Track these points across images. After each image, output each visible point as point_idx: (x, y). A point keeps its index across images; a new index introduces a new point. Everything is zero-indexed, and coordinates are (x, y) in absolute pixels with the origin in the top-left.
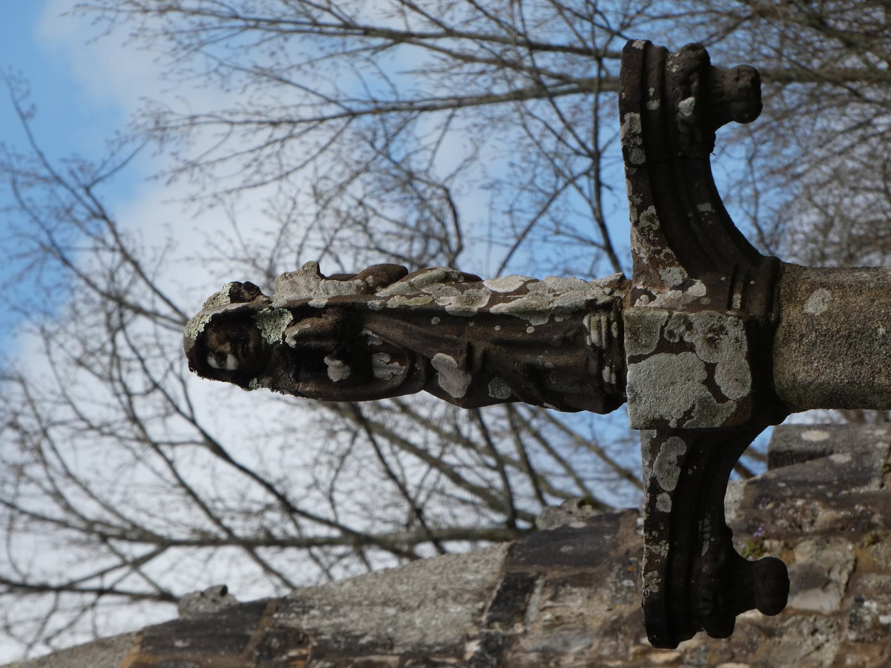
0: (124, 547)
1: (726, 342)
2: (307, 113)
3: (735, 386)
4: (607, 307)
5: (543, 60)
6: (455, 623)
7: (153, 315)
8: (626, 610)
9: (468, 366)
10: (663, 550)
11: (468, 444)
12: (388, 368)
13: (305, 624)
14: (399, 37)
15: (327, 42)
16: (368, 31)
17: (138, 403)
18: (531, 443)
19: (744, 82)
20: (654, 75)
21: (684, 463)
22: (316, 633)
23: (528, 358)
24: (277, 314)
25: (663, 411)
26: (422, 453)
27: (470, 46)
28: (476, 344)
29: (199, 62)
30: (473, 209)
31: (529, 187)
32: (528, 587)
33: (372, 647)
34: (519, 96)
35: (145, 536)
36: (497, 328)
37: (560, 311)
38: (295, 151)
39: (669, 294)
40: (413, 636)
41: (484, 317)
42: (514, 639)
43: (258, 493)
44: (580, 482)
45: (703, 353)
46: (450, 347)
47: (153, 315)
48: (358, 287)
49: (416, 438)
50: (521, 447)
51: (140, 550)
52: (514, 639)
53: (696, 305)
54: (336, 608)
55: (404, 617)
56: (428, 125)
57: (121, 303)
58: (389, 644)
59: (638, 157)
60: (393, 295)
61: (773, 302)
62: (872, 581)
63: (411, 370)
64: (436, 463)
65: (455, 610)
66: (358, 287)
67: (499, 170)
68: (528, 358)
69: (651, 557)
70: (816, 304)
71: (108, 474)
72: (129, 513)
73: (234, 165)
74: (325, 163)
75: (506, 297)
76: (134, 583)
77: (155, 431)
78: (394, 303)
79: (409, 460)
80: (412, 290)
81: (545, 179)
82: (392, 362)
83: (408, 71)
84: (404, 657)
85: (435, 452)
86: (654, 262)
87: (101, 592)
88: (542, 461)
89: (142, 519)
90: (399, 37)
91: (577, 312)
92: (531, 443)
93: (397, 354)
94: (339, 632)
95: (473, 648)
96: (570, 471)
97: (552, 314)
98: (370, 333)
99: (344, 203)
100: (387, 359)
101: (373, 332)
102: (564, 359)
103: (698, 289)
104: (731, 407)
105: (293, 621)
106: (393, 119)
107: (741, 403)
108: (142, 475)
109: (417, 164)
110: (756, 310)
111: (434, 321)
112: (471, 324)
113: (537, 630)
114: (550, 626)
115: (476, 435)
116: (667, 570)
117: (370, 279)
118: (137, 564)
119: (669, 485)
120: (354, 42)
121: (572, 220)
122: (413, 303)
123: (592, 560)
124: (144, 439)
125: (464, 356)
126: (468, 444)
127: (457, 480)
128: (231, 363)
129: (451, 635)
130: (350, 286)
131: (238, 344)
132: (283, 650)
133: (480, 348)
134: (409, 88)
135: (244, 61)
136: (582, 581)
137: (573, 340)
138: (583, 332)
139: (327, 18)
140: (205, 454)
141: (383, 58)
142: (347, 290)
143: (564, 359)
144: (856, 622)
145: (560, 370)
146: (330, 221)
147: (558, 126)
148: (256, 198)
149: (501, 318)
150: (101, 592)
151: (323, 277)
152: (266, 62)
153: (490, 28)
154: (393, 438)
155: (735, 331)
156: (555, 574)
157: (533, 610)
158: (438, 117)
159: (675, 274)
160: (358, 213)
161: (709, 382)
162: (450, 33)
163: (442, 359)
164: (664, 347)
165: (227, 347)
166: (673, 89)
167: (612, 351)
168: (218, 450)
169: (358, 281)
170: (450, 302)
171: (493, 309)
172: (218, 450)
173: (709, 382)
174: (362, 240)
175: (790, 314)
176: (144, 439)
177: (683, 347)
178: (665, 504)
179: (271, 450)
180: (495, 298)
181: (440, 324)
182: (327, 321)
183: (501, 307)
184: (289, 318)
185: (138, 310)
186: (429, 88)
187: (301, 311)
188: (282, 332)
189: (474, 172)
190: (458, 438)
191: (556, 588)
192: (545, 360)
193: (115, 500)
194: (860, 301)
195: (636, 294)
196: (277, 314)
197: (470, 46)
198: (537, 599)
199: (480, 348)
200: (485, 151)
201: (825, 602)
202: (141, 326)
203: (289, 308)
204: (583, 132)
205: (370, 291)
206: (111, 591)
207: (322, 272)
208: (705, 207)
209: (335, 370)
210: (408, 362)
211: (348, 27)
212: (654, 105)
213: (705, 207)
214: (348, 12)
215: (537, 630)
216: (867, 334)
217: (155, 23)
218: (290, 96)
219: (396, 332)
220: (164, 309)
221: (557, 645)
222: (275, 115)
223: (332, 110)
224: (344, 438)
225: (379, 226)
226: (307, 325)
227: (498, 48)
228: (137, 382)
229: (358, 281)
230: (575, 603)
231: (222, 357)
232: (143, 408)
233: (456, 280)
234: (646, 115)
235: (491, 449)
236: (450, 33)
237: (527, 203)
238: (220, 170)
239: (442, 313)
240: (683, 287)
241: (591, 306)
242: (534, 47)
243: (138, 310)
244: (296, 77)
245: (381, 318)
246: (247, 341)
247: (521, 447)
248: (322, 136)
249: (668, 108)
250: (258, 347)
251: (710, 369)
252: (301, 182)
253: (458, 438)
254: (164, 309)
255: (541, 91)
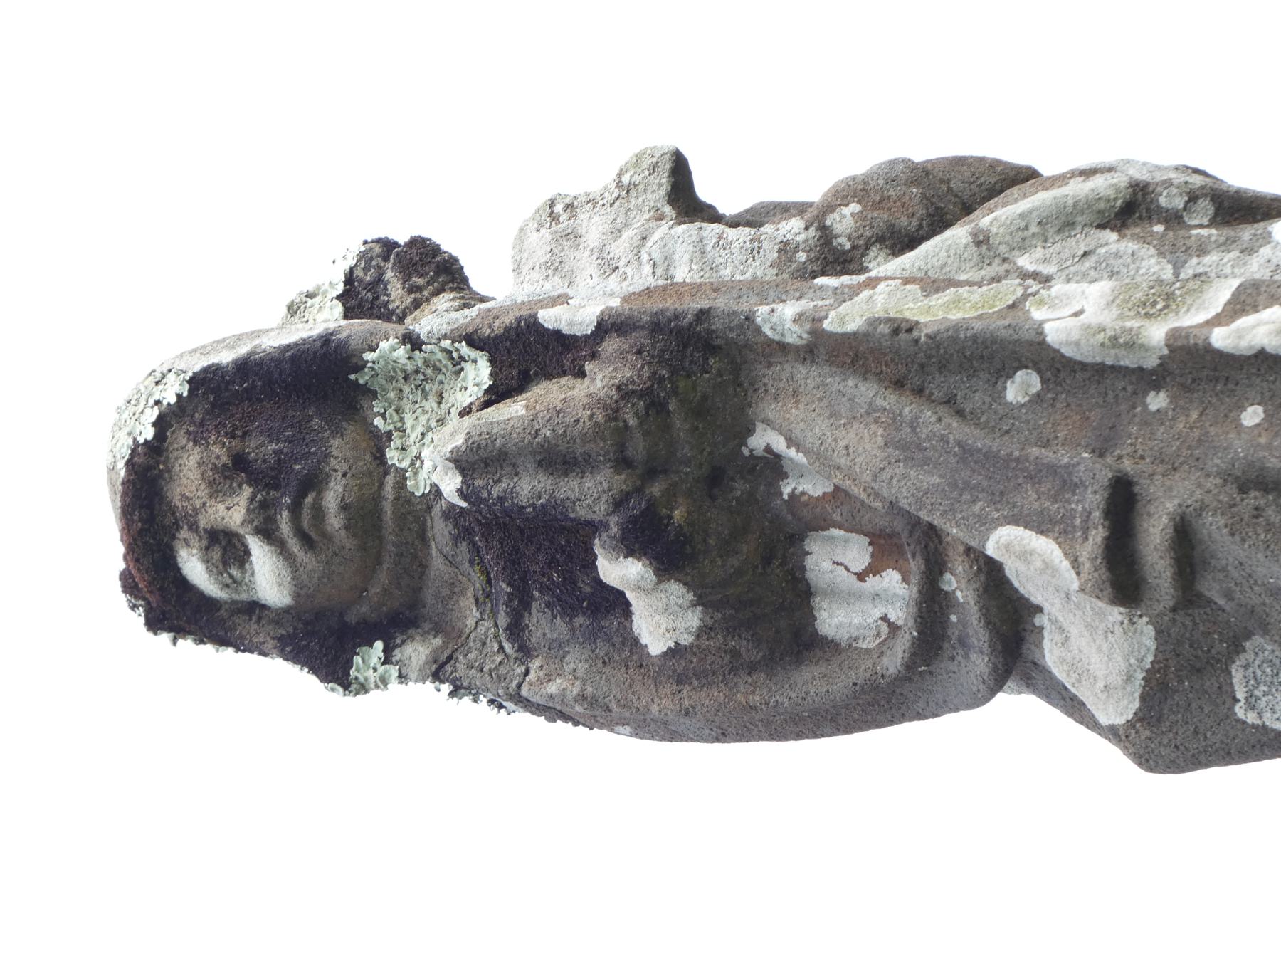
12: (860, 600)
28: (435, 406)
36: (1252, 416)
48: (786, 249)
63: (932, 604)
66: (786, 249)
80: (982, 261)
82: (874, 569)
98: (779, 444)
100: (857, 553)
111: (1020, 387)
112: (1157, 401)
117: (844, 221)
125: (1098, 535)
130: (754, 251)
131: (281, 488)
151: (708, 214)
165: (233, 512)
169: (793, 228)
171: (1221, 338)
181: (1038, 398)
184: (479, 372)
203: (473, 340)
207: (704, 190)
209: (661, 618)
210: (916, 565)
229: (793, 228)
231: (226, 550)
233: (1174, 219)
245: (809, 376)
246: (313, 482)
250: (363, 515)
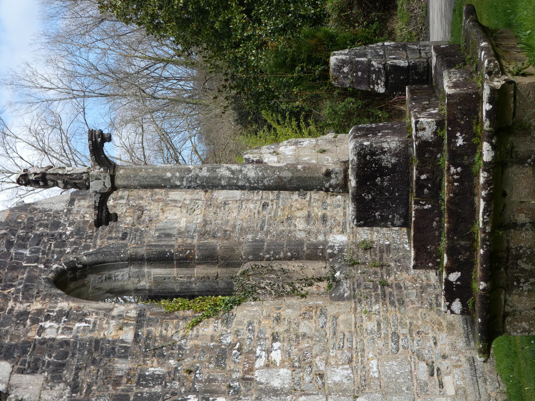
0: (6, 174)
1: (107, 178)
2: (35, 101)
3: (108, 185)
4: (87, 173)
5: (75, 92)
6: (62, 206)
7: (10, 136)
8: (91, 204)
9: (64, 182)
10: (97, 212)
11: (64, 156)
12: (50, 183)
13: (37, 207)
14: (50, 89)
15: (38, 89)
16: (45, 88)
17: (8, 151)
18: (74, 156)
19: (109, 136)
20: (94, 135)
21: (100, 198)
22: (39, 208)
23: (74, 181)
24: (31, 174)
25: (96, 190)
26: (56, 158)
27: (62, 90)
29: (17, 93)
30: (63, 117)
31: (73, 114)
32: (75, 200)
33: (48, 211)
34: (71, 98)
35: (10, 172)
37: (79, 173)
38: (33, 108)
39: (97, 170)
40: (56, 209)
41: (66, 175)
42: (72, 209)
43: (29, 165)
44: (82, 162)
45: (103, 180)
46: (61, 179)
47: (10, 136)
49: (55, 155)
50: (73, 156)
51: (9, 175)
52: (72, 209)
53: (102, 172)
54: (42, 204)
55: (54, 205)
56: (56, 103)
57: (5, 134)
58: (51, 210)
59: (91, 148)
60: (51, 171)
61: (114, 172)
62: (131, 198)
64: (58, 159)
65: (62, 204)
67: (68, 111)
68: (74, 181)
69: (95, 213)
70: (121, 172)
71: (3, 162)
72: (7, 169)
73: (23, 110)
74: (38, 110)
75: (70, 171)
76: (8, 180)
77: (11, 155)
78: (51, 172)
79: (54, 159)
81: (75, 112)
83: (51, 94)
84: (54, 212)
85: (58, 157)
86: (94, 165)
87: (3, 182)
88: (76, 159)
89: (9, 170)
90: (50, 89)
91: (82, 174)
92: (74, 156)
93: (52, 181)
94: (43, 208)
95: (65, 210)
96: (81, 160)
97: (77, 174)
99: (42, 117)
101: (48, 177)
102: (80, 181)
103: (102, 169)
104: (108, 189)
105: (35, 206)
106: (50, 102)
107: (109, 188)
108: (9, 162)
109: (54, 110)
110: (112, 173)
113: (76, 207)
114: (78, 207)
115: (65, 155)
116: (98, 215)
118: (8, 177)
119: (98, 201)
120: (43, 90)
121: (80, 119)
122: (55, 172)
123: (85, 195)
124: (9, 157)
126: (64, 156)
127: (62, 162)
128: (24, 182)
129: (62, 208)
131: (25, 179)
132: (34, 211)
133: (66, 180)
134: (52, 97)
135: (25, 93)
136: (83, 199)
137: (81, 178)
138: (83, 177)
139: (38, 86)
140: (20, 159)
141: (48, 92)
142: (43, 170)
143: (80, 181)
144: (129, 205)
145: (79, 183)
146: (40, 120)
147: (77, 104)
148: (27, 115)
149: (69, 175)
150: (3, 182)
152: (28, 93)
153: (66, 87)
154: (51, 156)
155: (108, 177)
156: (79, 198)
157: (75, 204)
158: (58, 102)
159: (98, 167)
160: (44, 119)
161: (104, 185)
162: (59, 88)
163: (59, 181)
164: (96, 179)
166: (97, 137)
167: (88, 180)
168: (22, 158)
170: (60, 172)
172: (22, 158)
173: (104, 185)
174: (45, 123)
175: (117, 173)
176: (9, 157)
177: (99, 179)
178: (97, 205)
179: (31, 158)
180: (68, 171)
182: (40, 176)
183: (69, 173)
185: (8, 135)
186: (55, 97)
187: (35, 174)
188: (32, 177)
189: (64, 111)
190: (62, 155)
191: (79, 200)
192: (77, 181)
193: (5, 167)
194: (129, 171)
195: (91, 170)
196: (31, 174)
197: (62, 90)
198: (76, 202)
199: (66, 180)
200: (65, 108)
201: (124, 201)
202: (8, 138)
204: (82, 104)
205: (47, 170)
206: (4, 182)
208: (103, 156)
209: (41, 183)
211: (42, 87)
212: (94, 140)
213: (103, 156)
214: (42, 85)
215: (76, 207)
216: (130, 177)
217: (9, 87)
218: (32, 98)
219: (51, 177)
220: (12, 135)
221: (80, 210)
222: (30, 102)
223: (39, 101)
224: (43, 156)
225: (48, 121)
226: (36, 176)
227: (67, 91)
228: (8, 147)
230: (82, 202)
231: (22, 182)
232: (9, 151)
234: (92, 141)
235: (68, 157)
236: (59, 88)
237: (73, 117)
238: (21, 111)
239: (59, 174)
240: (99, 169)
241: (84, 173)
242: (73, 90)
243: (8, 135)
244: (33, 95)
247: (73, 156)
248: (38, 105)
249: (96, 140)
251: (104, 183)
252: (35, 113)
253: (62, 155)
254: (12, 135)
255: (74, 97)
